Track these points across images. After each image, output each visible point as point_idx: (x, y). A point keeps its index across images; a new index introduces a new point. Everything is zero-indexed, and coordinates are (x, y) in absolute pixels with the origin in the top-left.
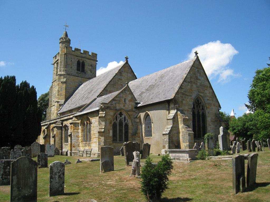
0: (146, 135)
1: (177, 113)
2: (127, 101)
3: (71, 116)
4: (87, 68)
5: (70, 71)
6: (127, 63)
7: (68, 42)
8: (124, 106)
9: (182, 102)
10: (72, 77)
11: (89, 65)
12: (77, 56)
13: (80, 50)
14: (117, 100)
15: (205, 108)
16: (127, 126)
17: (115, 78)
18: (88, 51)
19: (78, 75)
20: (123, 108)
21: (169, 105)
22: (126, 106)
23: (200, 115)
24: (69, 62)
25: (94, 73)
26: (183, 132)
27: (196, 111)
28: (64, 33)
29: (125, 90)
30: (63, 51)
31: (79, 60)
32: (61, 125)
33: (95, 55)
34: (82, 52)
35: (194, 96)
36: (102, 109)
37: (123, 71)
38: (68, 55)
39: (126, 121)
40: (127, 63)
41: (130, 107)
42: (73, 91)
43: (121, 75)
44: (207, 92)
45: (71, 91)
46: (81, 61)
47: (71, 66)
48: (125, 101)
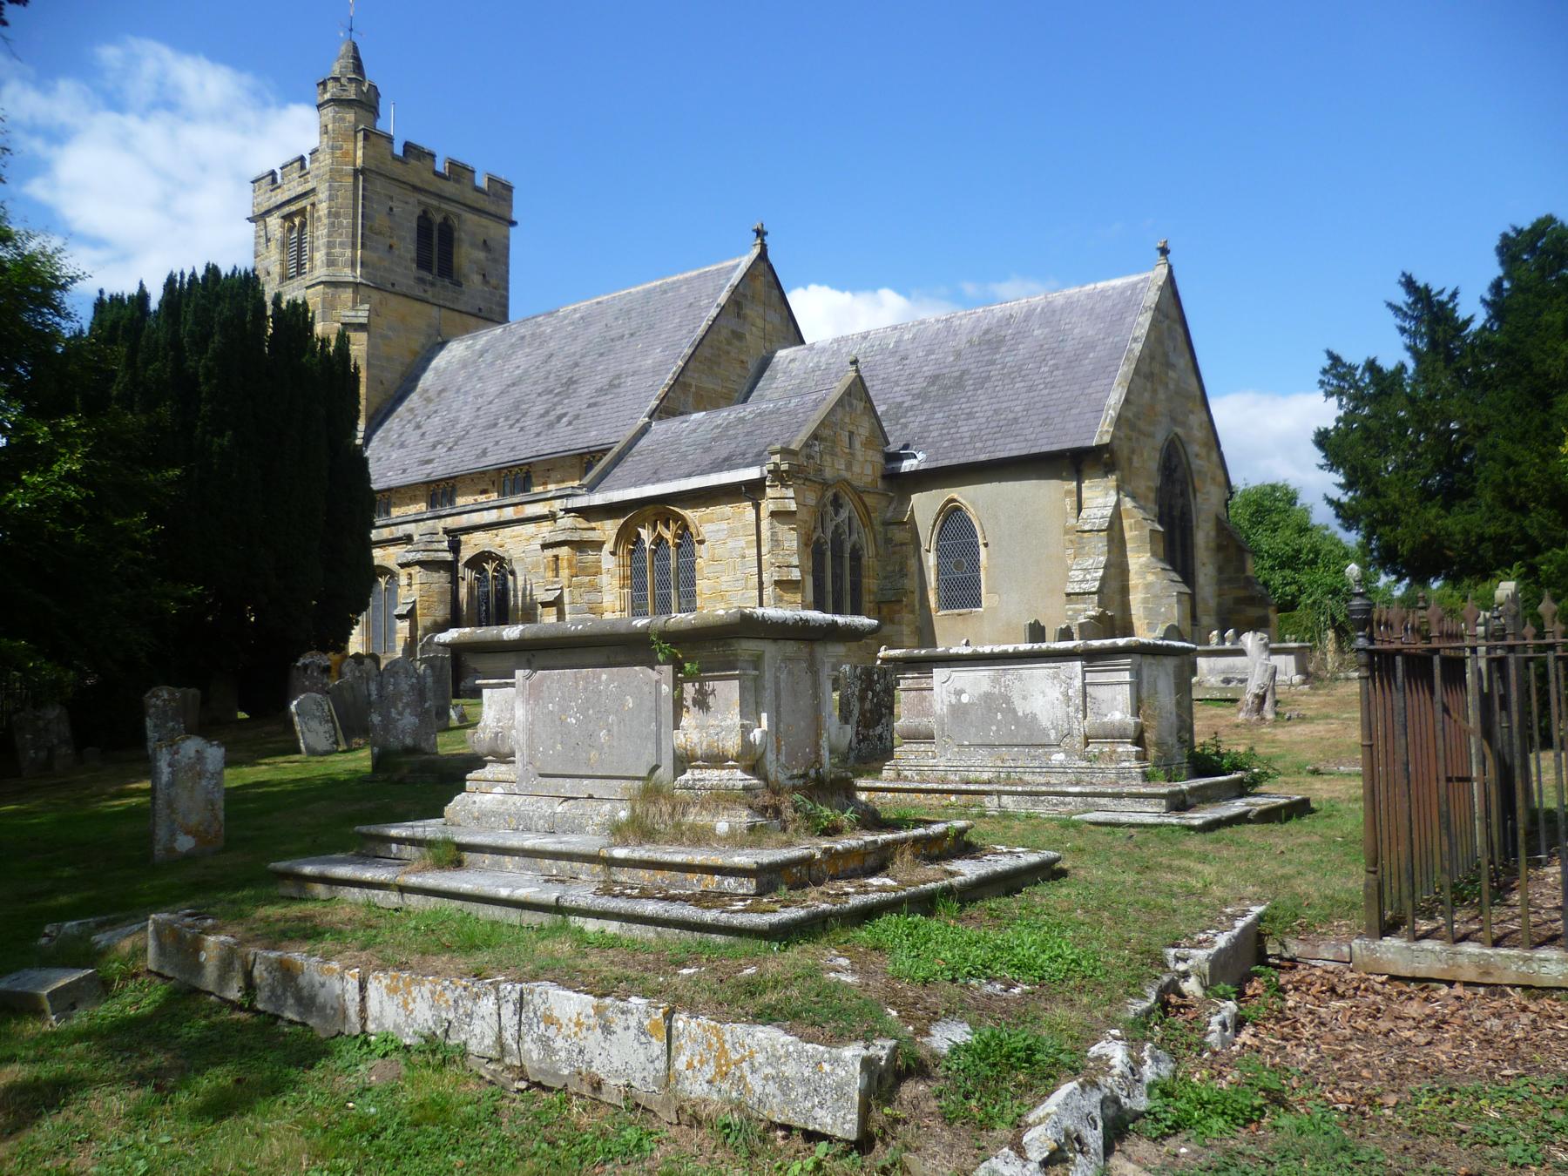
0: (947, 603)
1: (1118, 504)
3: (557, 505)
4: (467, 256)
6: (763, 256)
7: (368, 103)
8: (849, 467)
9: (1130, 460)
11: (473, 245)
12: (415, 188)
13: (432, 156)
14: (825, 440)
16: (856, 556)
17: (715, 328)
22: (856, 469)
24: (381, 220)
26: (1148, 587)
28: (344, 48)
30: (346, 154)
31: (425, 212)
32: (449, 556)
33: (501, 191)
34: (440, 166)
35: (1160, 439)
36: (779, 477)
37: (749, 294)
40: (763, 256)
44: (1196, 419)
46: (438, 219)
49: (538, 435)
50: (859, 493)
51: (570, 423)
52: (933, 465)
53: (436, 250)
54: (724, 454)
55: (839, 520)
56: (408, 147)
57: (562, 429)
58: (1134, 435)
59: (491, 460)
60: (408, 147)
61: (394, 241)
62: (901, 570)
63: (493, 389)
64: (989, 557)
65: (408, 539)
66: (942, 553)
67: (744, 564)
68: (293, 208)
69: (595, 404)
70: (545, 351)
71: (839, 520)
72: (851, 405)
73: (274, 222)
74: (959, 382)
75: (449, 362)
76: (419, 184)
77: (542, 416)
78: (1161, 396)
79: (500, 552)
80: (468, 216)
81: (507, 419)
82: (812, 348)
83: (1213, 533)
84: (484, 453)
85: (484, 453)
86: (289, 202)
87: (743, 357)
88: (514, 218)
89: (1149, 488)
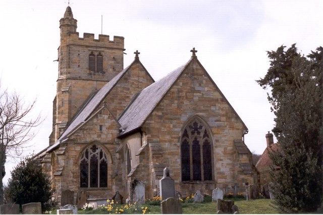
2: (104, 129)
8: (99, 136)
10: (80, 82)
12: (87, 46)
15: (211, 133)
16: (104, 164)
18: (107, 34)
20: (97, 139)
22: (103, 136)
23: (199, 145)
27: (191, 141)
38: (74, 48)
39: (103, 157)
41: (110, 138)
45: (78, 105)
46: (96, 54)
48: (101, 129)
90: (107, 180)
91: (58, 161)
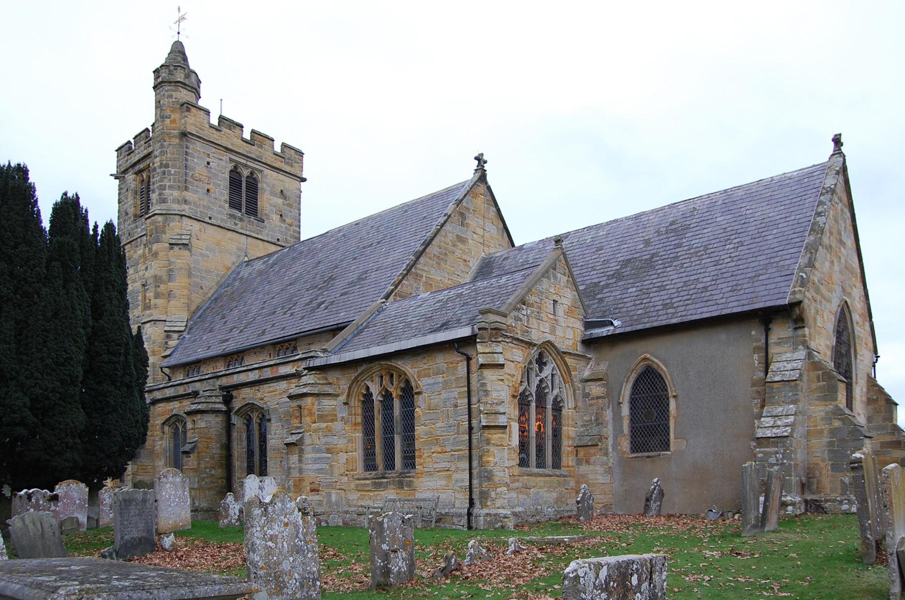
4: (267, 201)
5: (204, 206)
8: (553, 331)
11: (273, 193)
12: (227, 149)
14: (532, 305)
16: (557, 408)
19: (236, 224)
21: (767, 331)
22: (559, 332)
25: (291, 225)
29: (555, 269)
32: (224, 408)
42: (218, 283)
43: (462, 225)
46: (246, 173)
47: (207, 187)
49: (303, 317)
50: (562, 354)
51: (326, 308)
52: (629, 329)
53: (244, 195)
54: (443, 320)
55: (543, 375)
56: (222, 119)
57: (321, 313)
58: (819, 298)
59: (267, 338)
60: (222, 119)
61: (211, 187)
62: (597, 420)
63: (276, 288)
64: (678, 407)
65: (195, 394)
66: (632, 408)
67: (456, 413)
68: (142, 166)
69: (346, 293)
70: (316, 260)
71: (543, 375)
72: (555, 277)
73: (130, 177)
74: (649, 263)
75: (250, 274)
76: (230, 147)
77: (308, 304)
78: (836, 267)
79: (260, 404)
80: (267, 172)
81: (283, 308)
82: (521, 248)
83: (865, 389)
84: (263, 333)
85: (263, 333)
86: (138, 162)
87: (467, 258)
88: (304, 176)
89: (827, 346)
90: (560, 448)
91: (484, 385)
